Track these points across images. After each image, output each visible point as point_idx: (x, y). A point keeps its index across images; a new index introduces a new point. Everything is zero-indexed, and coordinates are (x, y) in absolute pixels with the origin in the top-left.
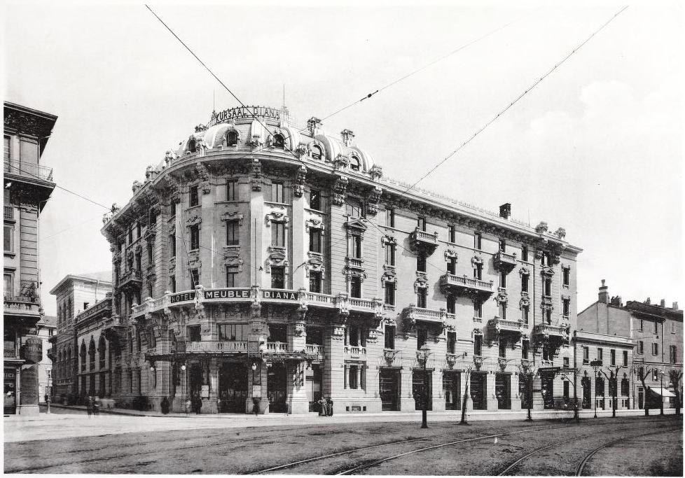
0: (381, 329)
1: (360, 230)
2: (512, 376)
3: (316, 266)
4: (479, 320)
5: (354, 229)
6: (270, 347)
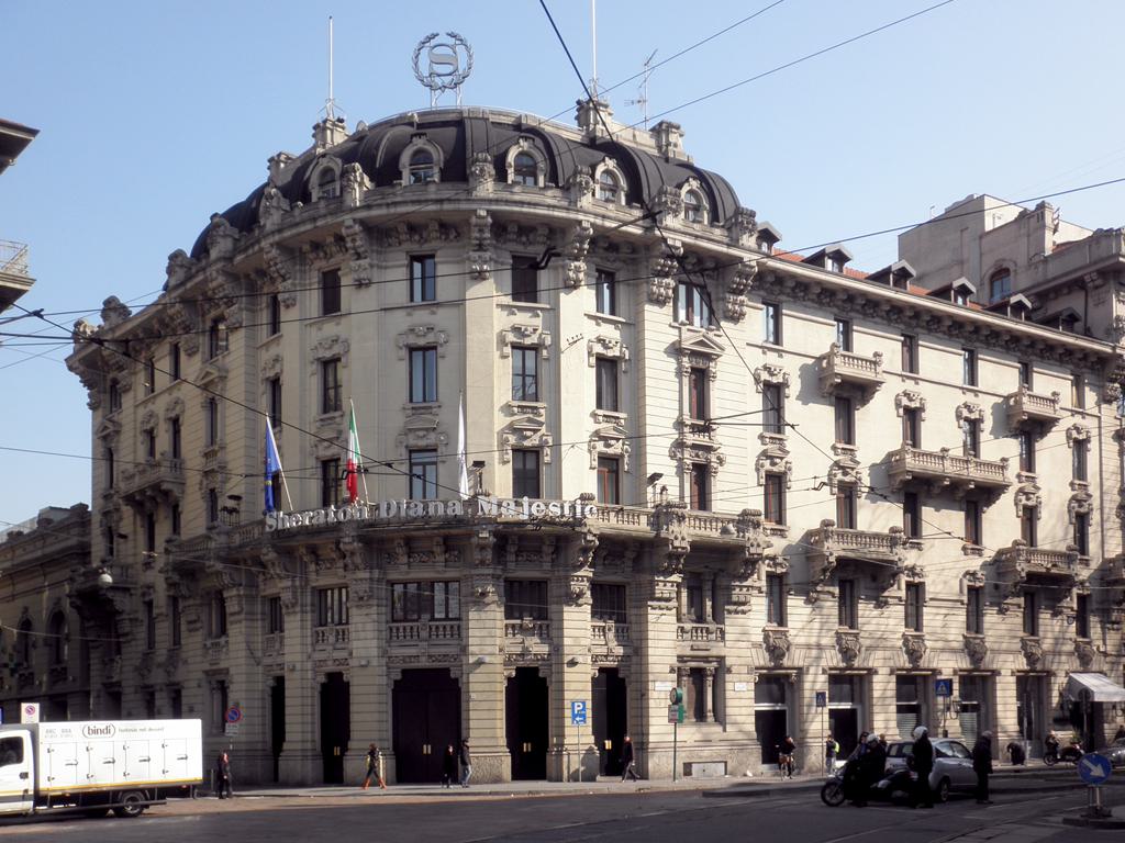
0: (759, 580)
1: (708, 357)
2: (876, 678)
3: (613, 442)
4: (979, 552)
5: (694, 354)
6: (510, 631)
